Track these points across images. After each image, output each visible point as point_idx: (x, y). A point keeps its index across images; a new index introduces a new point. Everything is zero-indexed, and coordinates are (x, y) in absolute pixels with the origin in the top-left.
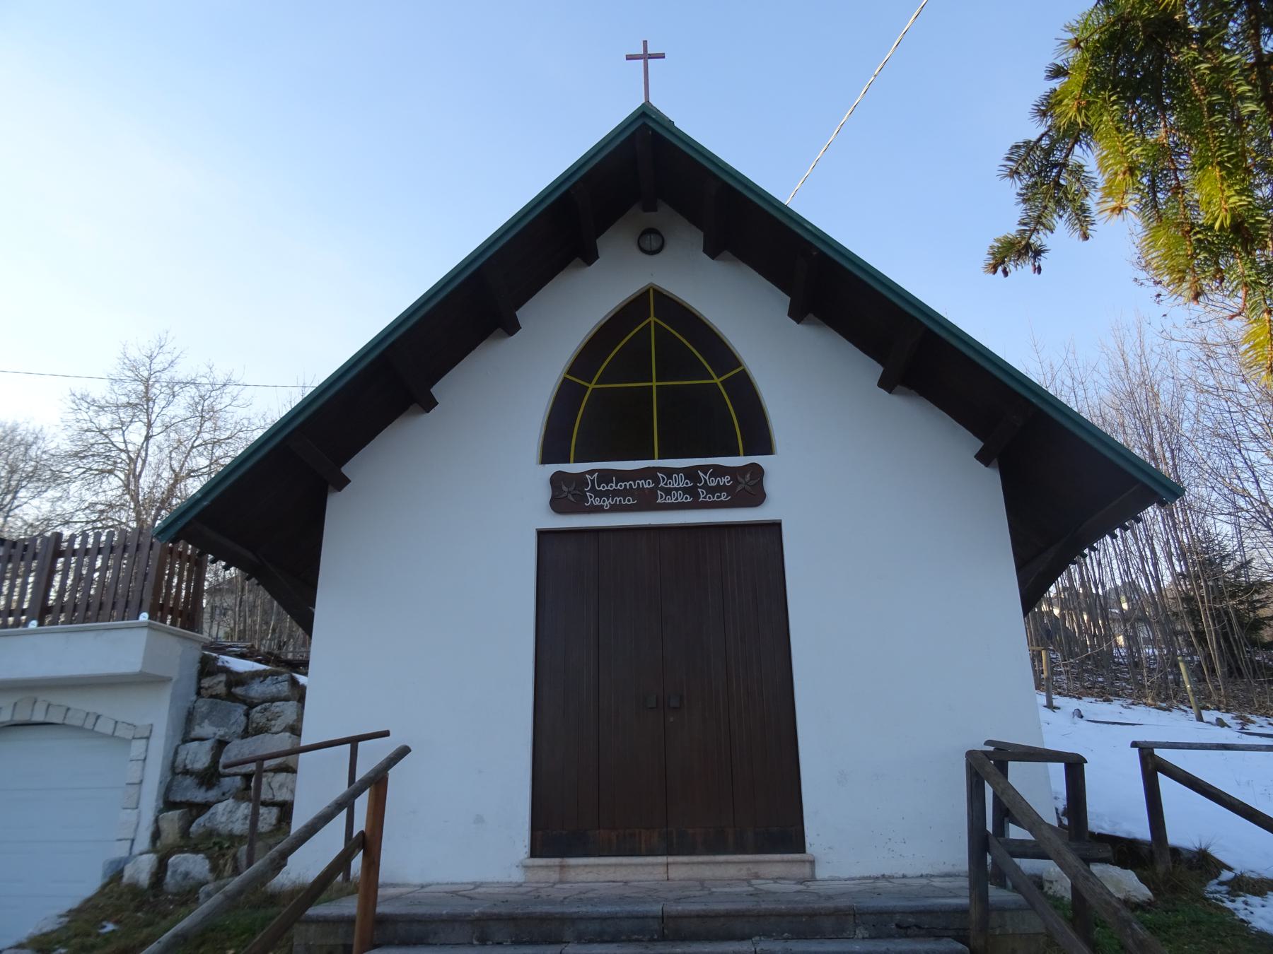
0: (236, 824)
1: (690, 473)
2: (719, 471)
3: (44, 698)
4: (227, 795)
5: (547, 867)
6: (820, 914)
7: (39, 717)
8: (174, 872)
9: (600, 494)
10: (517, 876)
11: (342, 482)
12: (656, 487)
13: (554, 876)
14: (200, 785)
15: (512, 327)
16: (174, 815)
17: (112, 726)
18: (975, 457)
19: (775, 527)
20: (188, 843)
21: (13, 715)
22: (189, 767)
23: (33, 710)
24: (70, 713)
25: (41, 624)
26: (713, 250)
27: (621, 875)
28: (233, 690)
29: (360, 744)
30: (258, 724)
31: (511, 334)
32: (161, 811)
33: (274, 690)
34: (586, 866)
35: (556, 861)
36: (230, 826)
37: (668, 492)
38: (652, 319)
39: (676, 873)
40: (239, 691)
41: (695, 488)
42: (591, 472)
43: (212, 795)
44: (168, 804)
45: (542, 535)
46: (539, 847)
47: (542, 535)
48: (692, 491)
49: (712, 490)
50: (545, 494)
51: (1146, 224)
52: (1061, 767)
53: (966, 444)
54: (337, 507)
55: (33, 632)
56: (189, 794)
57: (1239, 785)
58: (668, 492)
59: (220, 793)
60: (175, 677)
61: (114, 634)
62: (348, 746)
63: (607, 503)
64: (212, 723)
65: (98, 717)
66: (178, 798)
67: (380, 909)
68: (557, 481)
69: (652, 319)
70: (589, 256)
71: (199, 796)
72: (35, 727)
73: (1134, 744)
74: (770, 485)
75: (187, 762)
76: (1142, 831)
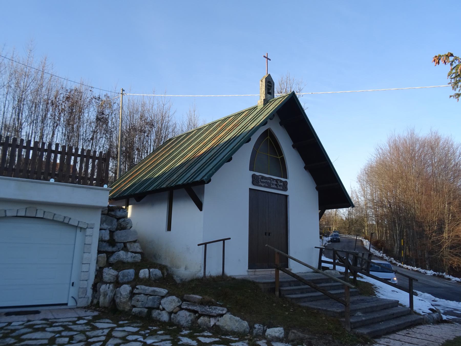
0: (129, 259)
1: (277, 180)
4: (120, 249)
5: (252, 271)
6: (260, 283)
8: (152, 274)
9: (262, 182)
10: (246, 273)
13: (253, 273)
14: (110, 245)
16: (104, 255)
17: (77, 223)
18: (249, 170)
19: (286, 196)
20: (109, 264)
21: (25, 214)
22: (104, 239)
23: (36, 213)
24: (56, 216)
26: (281, 124)
27: (264, 273)
28: (110, 212)
29: (225, 241)
30: (124, 226)
33: (124, 214)
34: (259, 271)
35: (254, 270)
36: (127, 260)
38: (268, 137)
39: (258, 273)
40: (113, 213)
42: (260, 176)
43: (114, 249)
44: (99, 252)
46: (250, 267)
48: (276, 185)
50: (250, 179)
52: (123, 244)
53: (313, 185)
55: (52, 184)
56: (106, 248)
59: (117, 249)
61: (94, 191)
64: (107, 224)
65: (70, 219)
66: (102, 250)
67: (280, 280)
68: (253, 176)
69: (268, 137)
71: (110, 249)
72: (28, 218)
75: (103, 237)
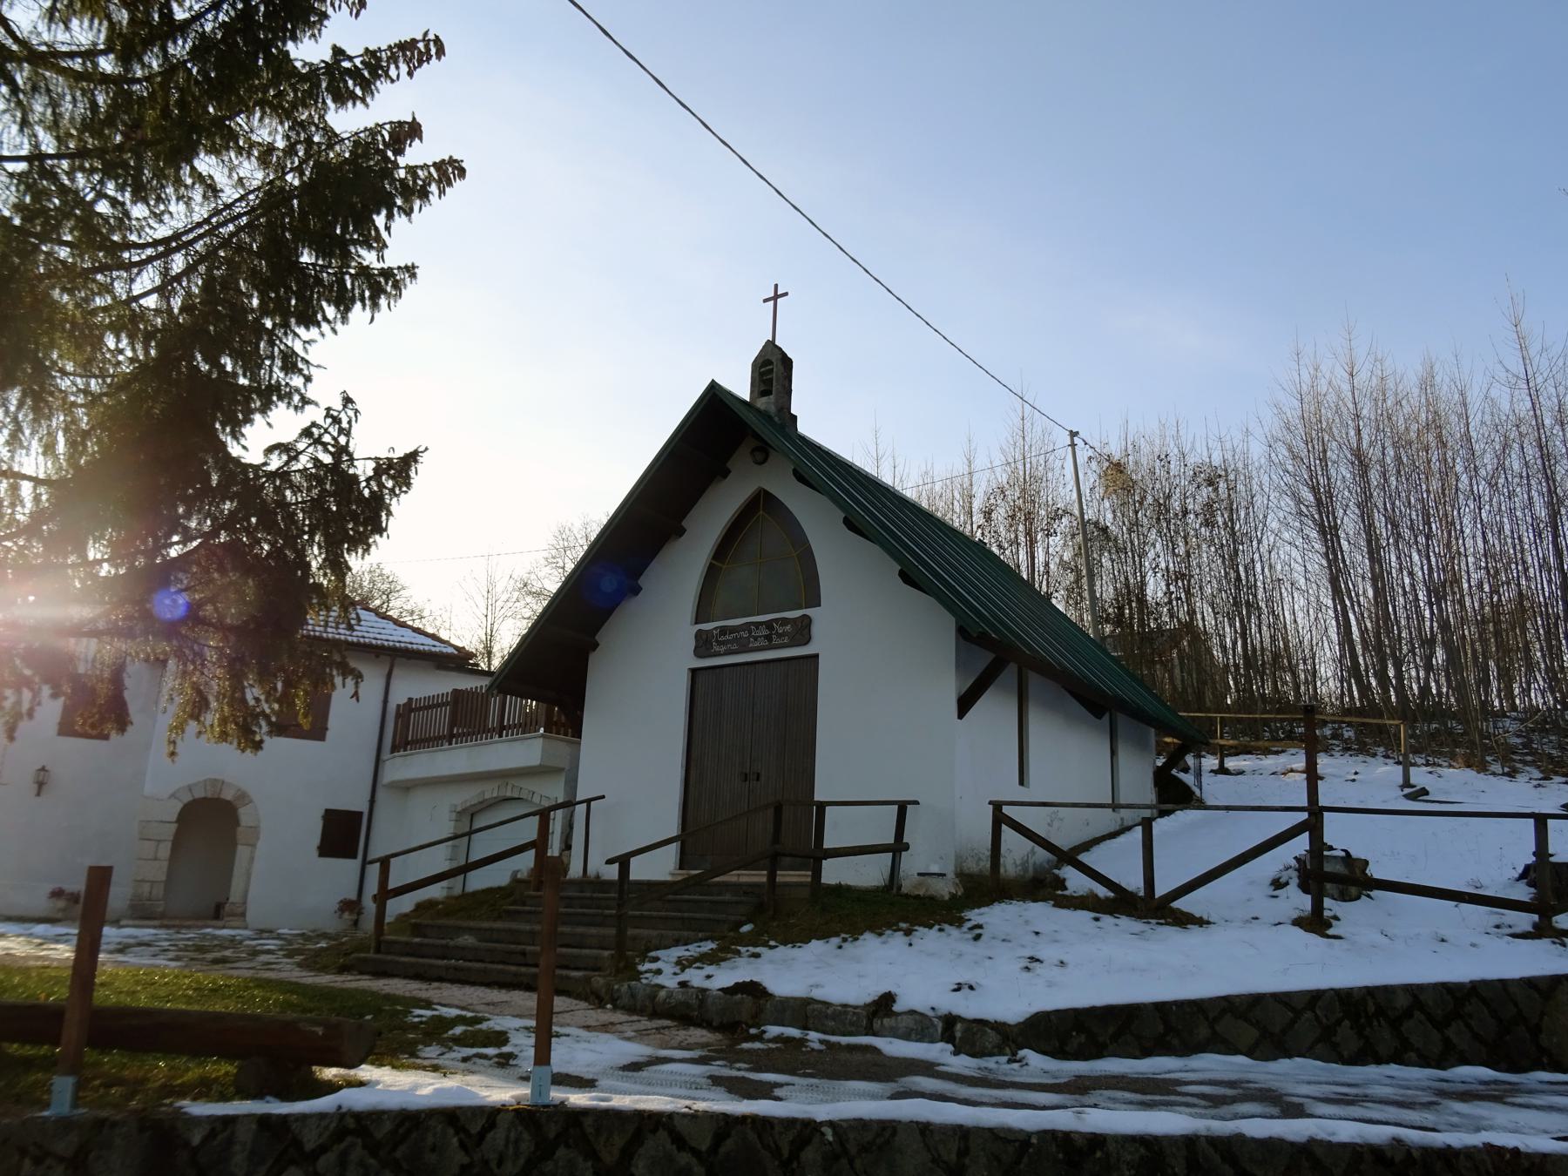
1: (769, 625)
2: (785, 621)
3: (512, 782)
7: (509, 794)
9: (720, 643)
11: (595, 646)
12: (750, 636)
15: (681, 532)
25: (501, 736)
29: (592, 803)
31: (681, 536)
32: (563, 850)
37: (756, 639)
41: (771, 634)
42: (716, 628)
45: (694, 672)
47: (694, 672)
49: (780, 636)
51: (1454, 428)
54: (595, 660)
57: (41, 785)
58: (756, 639)
60: (567, 768)
62: (585, 805)
63: (723, 649)
68: (699, 634)
70: (725, 473)
73: (990, 803)
74: (816, 630)
76: (674, 848)
